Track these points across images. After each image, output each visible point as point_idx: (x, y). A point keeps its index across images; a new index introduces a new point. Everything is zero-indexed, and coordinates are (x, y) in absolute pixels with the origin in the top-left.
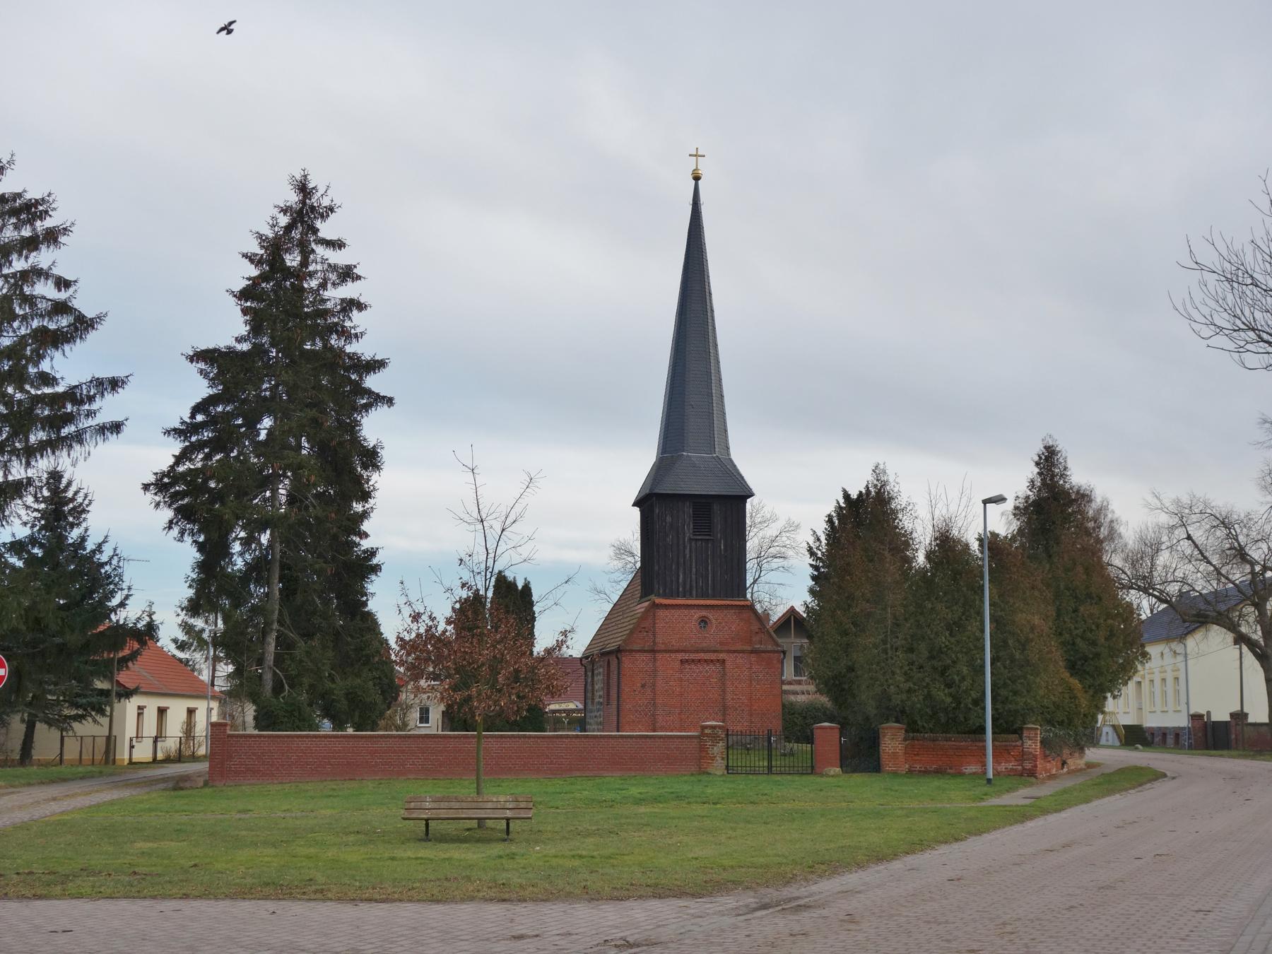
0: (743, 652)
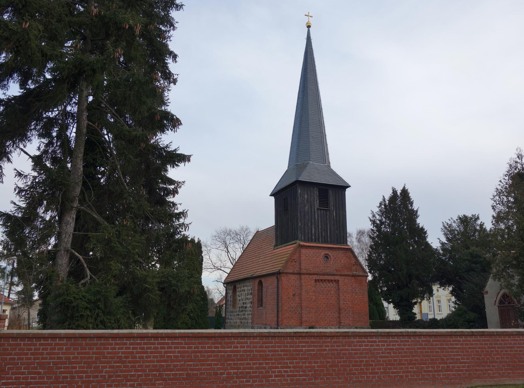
0: (348, 275)
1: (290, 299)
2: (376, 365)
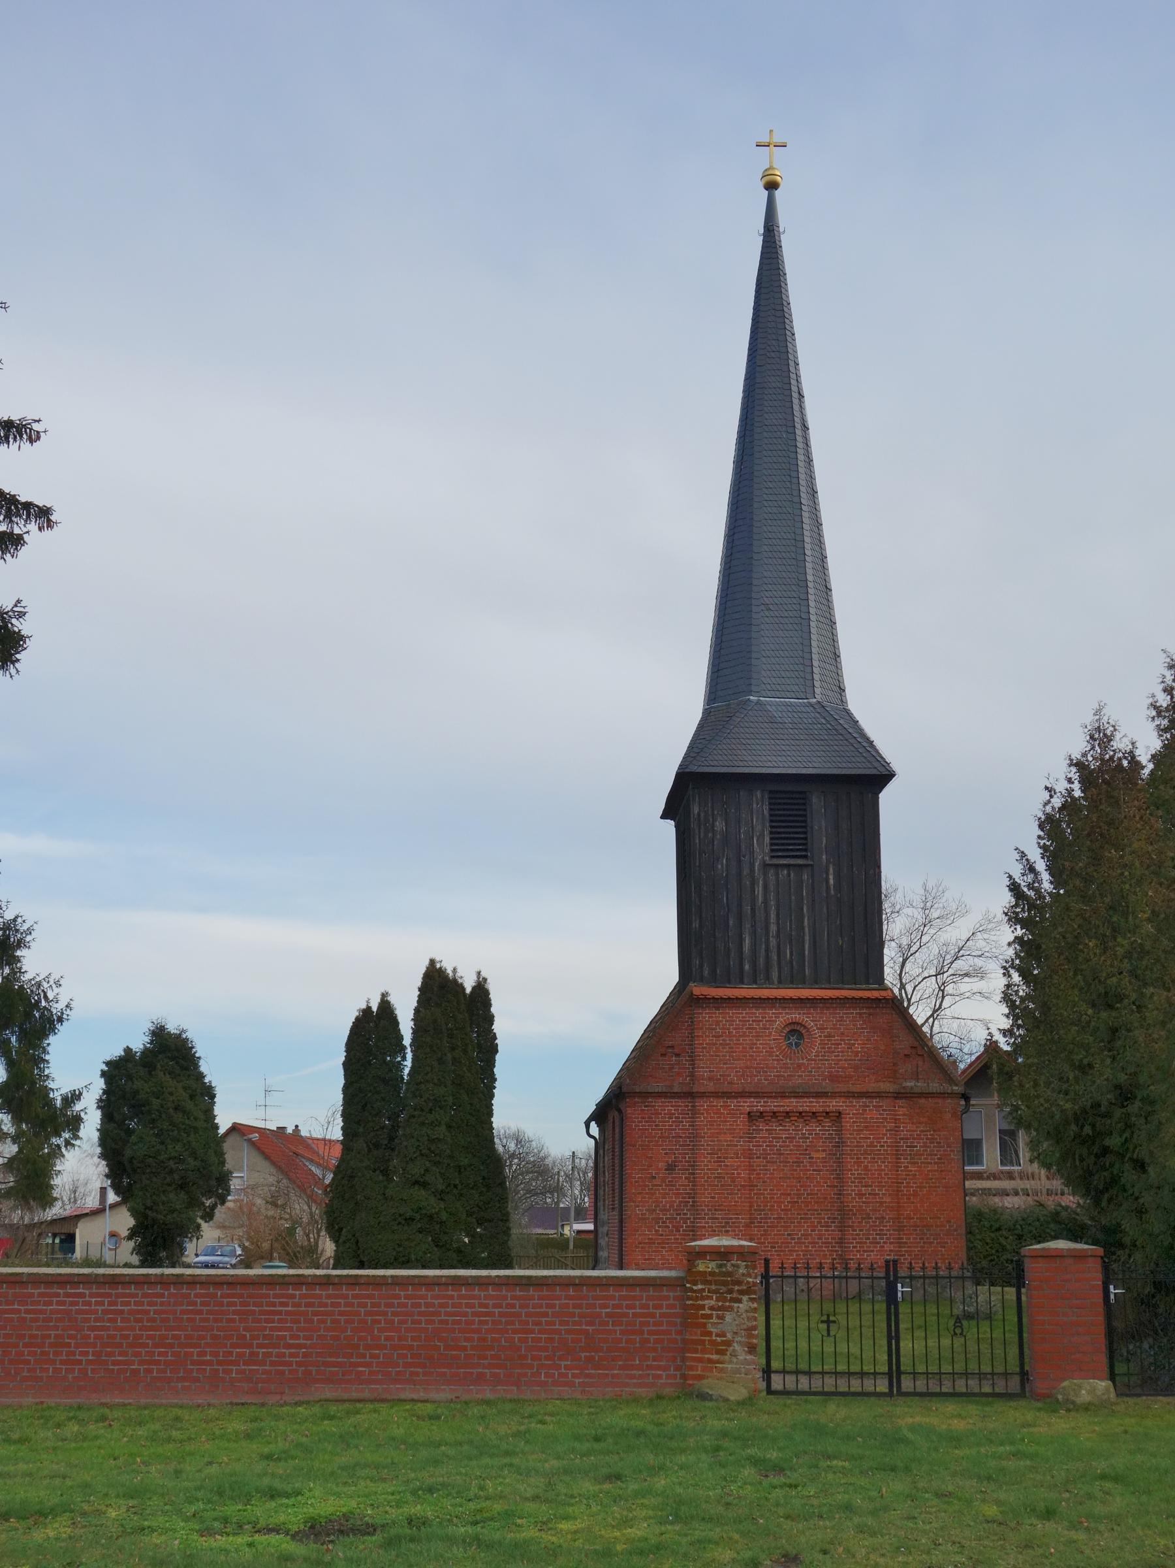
0: (878, 1095)
1: (657, 1182)
2: (77, 1346)
